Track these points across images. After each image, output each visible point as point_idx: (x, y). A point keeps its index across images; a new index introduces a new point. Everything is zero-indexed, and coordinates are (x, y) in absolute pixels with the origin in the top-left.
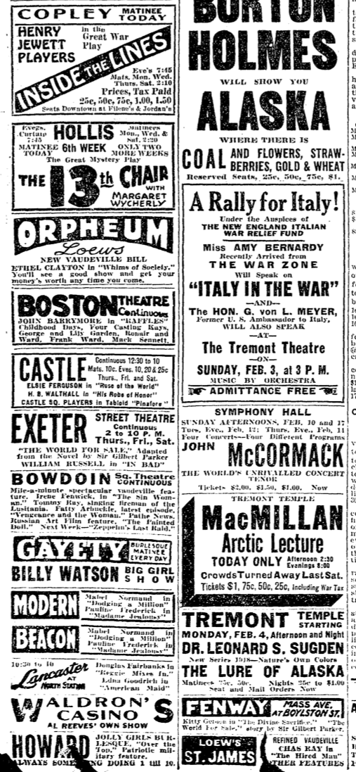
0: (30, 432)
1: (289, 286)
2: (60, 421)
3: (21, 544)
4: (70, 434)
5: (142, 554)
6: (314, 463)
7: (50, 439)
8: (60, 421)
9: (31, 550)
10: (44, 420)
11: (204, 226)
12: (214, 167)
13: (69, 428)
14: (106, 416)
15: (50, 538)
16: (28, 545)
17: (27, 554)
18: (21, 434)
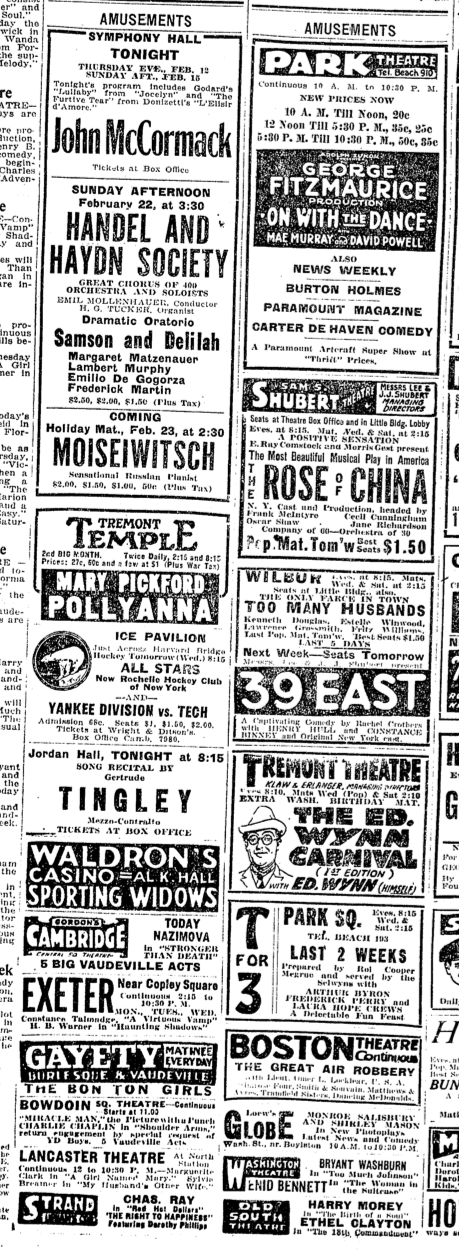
0: (45, 998)
1: (287, 1119)
2: (82, 987)
3: (30, 1051)
4: (94, 1003)
5: (178, 1055)
6: (87, 236)
7: (70, 1007)
8: (82, 987)
9: (41, 1059)
10: (62, 984)
11: (310, 935)
12: (76, 271)
13: (93, 995)
14: (146, 1157)
15: (62, 1044)
16: (38, 1052)
17: (36, 1063)
18: (34, 1002)
